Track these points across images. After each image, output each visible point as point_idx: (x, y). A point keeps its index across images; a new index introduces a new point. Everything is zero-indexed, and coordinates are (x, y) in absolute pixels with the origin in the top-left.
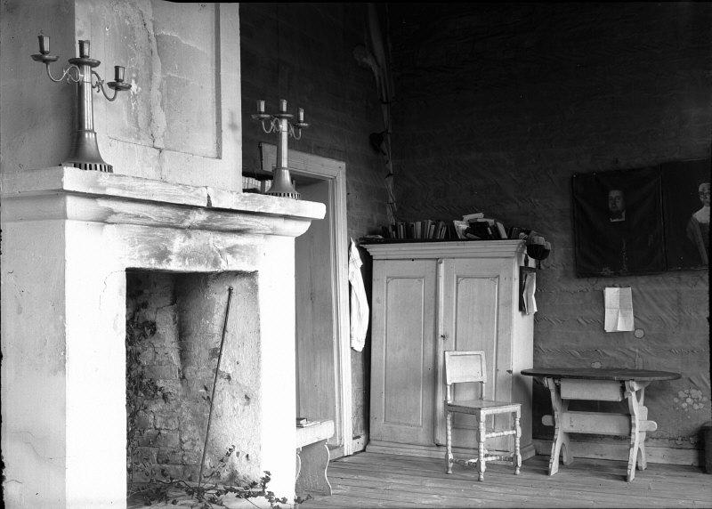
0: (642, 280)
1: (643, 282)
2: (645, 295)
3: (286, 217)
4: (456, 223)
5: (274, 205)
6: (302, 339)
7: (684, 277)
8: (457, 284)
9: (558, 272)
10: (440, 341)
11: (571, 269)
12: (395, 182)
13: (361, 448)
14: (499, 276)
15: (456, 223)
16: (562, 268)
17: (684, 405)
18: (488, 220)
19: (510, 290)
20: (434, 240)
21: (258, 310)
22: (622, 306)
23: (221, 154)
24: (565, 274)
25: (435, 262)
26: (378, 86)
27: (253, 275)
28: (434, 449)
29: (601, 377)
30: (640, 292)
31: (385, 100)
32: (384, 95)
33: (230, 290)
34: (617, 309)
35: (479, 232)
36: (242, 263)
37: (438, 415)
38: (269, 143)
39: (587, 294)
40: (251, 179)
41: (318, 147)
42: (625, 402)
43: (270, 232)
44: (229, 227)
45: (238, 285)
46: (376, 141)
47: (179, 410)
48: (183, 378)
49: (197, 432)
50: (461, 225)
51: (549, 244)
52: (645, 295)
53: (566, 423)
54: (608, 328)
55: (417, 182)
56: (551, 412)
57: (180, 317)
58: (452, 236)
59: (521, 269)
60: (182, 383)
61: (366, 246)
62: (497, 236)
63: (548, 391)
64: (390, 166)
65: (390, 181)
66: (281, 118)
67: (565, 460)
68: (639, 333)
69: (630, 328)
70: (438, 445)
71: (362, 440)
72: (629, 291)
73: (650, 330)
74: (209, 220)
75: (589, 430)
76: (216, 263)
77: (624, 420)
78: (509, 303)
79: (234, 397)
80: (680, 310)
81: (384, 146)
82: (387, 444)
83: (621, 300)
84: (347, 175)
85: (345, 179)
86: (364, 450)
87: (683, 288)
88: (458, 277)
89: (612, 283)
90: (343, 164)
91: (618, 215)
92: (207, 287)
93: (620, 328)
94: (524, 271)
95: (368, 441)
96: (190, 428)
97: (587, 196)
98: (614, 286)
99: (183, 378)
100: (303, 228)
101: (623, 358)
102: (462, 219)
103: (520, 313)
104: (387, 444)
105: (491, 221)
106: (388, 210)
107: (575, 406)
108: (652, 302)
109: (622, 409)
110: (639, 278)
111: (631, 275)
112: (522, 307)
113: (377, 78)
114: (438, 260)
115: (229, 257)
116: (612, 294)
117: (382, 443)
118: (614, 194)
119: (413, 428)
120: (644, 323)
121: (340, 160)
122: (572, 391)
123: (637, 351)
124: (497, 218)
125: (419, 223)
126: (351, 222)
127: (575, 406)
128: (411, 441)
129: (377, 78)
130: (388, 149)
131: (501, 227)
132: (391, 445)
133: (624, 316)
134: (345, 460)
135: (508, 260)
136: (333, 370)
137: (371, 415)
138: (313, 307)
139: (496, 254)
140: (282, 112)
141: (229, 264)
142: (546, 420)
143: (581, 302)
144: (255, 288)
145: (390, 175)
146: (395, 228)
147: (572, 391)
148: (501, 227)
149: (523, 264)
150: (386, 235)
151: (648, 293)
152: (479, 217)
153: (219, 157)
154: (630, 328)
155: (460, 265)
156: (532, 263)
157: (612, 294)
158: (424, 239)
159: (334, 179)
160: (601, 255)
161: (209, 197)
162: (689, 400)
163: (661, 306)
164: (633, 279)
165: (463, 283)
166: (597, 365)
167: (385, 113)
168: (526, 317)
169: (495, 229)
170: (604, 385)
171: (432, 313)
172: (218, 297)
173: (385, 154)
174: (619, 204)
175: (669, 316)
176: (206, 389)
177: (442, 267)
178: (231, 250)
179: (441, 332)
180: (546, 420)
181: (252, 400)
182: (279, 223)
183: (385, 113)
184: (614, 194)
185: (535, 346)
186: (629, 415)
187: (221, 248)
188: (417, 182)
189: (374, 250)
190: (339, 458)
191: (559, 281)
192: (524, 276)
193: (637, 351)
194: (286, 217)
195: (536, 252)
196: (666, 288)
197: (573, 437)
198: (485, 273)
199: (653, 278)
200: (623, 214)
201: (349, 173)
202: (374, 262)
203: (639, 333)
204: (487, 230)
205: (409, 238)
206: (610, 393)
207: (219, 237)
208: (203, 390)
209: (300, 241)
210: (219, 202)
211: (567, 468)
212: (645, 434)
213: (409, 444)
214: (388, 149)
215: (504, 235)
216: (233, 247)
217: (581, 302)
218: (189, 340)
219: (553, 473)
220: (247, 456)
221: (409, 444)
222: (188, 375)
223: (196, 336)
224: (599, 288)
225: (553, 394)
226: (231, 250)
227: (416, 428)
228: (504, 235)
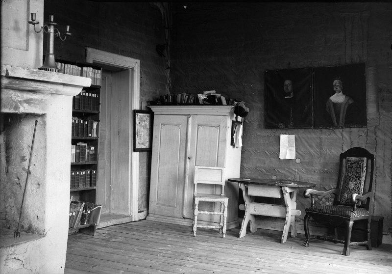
0: (301, 131)
1: (302, 132)
2: (303, 140)
3: (64, 85)
4: (199, 95)
5: (54, 77)
6: (113, 156)
7: (324, 130)
8: (198, 129)
9: (256, 124)
10: (188, 160)
11: (262, 123)
12: (171, 72)
13: (143, 218)
14: (219, 126)
15: (199, 95)
16: (258, 123)
17: (321, 202)
18: (216, 95)
19: (225, 134)
20: (187, 104)
21: (45, 136)
22: (290, 145)
23: (28, 48)
24: (259, 126)
25: (187, 117)
26: (163, 18)
27: (43, 115)
28: (182, 220)
29: (271, 184)
30: (299, 137)
31: (167, 26)
32: (167, 24)
33: (36, 122)
34: (287, 146)
35: (211, 101)
36: (35, 109)
37: (185, 202)
38: (91, 47)
39: (271, 138)
40: (74, 66)
41: (123, 51)
42: (282, 199)
43: (55, 92)
44: (24, 88)
45: (39, 120)
46: (160, 50)
47: (5, 190)
48: (7, 172)
49: (13, 203)
50: (202, 97)
51: (248, 109)
52: (303, 140)
53: (252, 209)
54: (282, 157)
55: (183, 72)
56: (243, 203)
57: (7, 138)
58: (196, 102)
59: (233, 121)
60: (7, 175)
61: (150, 107)
62: (220, 103)
63: (241, 191)
64: (169, 63)
65: (168, 71)
66: (50, 25)
67: (292, 234)
68: (298, 161)
69: (294, 158)
70: (184, 218)
71: (144, 213)
72: (293, 136)
73: (304, 159)
74: (10, 83)
75: (264, 214)
76: (16, 108)
77: (283, 208)
78: (225, 141)
79: (32, 184)
80: (321, 149)
81: (165, 51)
82: (158, 216)
83: (289, 141)
84: (141, 67)
85: (139, 70)
86: (145, 219)
87: (323, 137)
88: (198, 125)
89: (284, 132)
90: (138, 61)
91: (289, 94)
92: (20, 122)
93: (288, 158)
94: (235, 124)
95: (148, 214)
96: (10, 200)
97: (272, 81)
98: (286, 134)
99: (7, 172)
100: (78, 91)
101: (288, 174)
102: (203, 94)
103: (232, 147)
104: (158, 216)
105: (218, 95)
106: (166, 88)
107: (257, 200)
108: (306, 143)
109: (279, 202)
110: (299, 130)
111: (294, 128)
112: (232, 143)
113: (163, 14)
114: (188, 116)
115: (25, 105)
116: (284, 138)
117: (155, 216)
118: (287, 82)
119: (171, 208)
120: (302, 155)
121: (137, 58)
122: (254, 191)
123: (297, 170)
124: (223, 94)
125: (180, 95)
126: (142, 93)
127: (257, 200)
128: (170, 215)
129: (163, 14)
130: (168, 54)
131: (223, 99)
132: (160, 216)
133: (290, 150)
134: (132, 223)
135: (225, 117)
136: (128, 174)
137: (150, 199)
138: (119, 138)
139: (218, 114)
140: (51, 22)
141: (23, 109)
142: (241, 207)
143: (267, 142)
144: (44, 123)
145: (168, 68)
146: (167, 97)
147: (254, 191)
148: (223, 99)
149: (234, 119)
150: (161, 101)
151: (303, 138)
152: (213, 93)
153: (27, 50)
154: (294, 158)
155: (201, 119)
156: (240, 119)
157: (284, 138)
158: (182, 104)
159: (132, 69)
160: (279, 117)
161: (7, 70)
162: (324, 200)
163: (311, 146)
164: (296, 130)
165: (201, 129)
166: (274, 178)
167: (167, 34)
168: (236, 149)
169: (220, 99)
170: (272, 189)
171: (184, 144)
172: (27, 128)
173: (165, 56)
174: (290, 88)
175: (315, 152)
176: (18, 179)
177: (190, 119)
178: (28, 102)
179: (188, 155)
180: (241, 207)
181: (41, 186)
182: (60, 88)
183: (167, 34)
184: (287, 82)
185: (241, 165)
186: (285, 206)
187: (20, 100)
188: (183, 72)
189: (155, 109)
190: (129, 222)
191: (256, 130)
192: (234, 126)
193: (297, 170)
194: (64, 85)
195: (238, 111)
196: (314, 136)
197: (257, 217)
198: (213, 124)
199: (307, 130)
200: (292, 94)
201: (142, 66)
202: (155, 116)
203: (298, 161)
204: (215, 100)
205: (174, 103)
206: (274, 193)
207: (19, 94)
208: (17, 179)
209: (76, 101)
210: (15, 73)
211: (253, 234)
212: (294, 217)
213: (169, 216)
214: (168, 54)
215: (224, 102)
216: (28, 100)
217: (267, 142)
218: (11, 151)
219: (241, 236)
220: (38, 217)
221: (169, 216)
222: (10, 170)
223: (15, 149)
224: (277, 134)
225: (244, 193)
226: (28, 102)
227: (173, 208)
228: (224, 102)
